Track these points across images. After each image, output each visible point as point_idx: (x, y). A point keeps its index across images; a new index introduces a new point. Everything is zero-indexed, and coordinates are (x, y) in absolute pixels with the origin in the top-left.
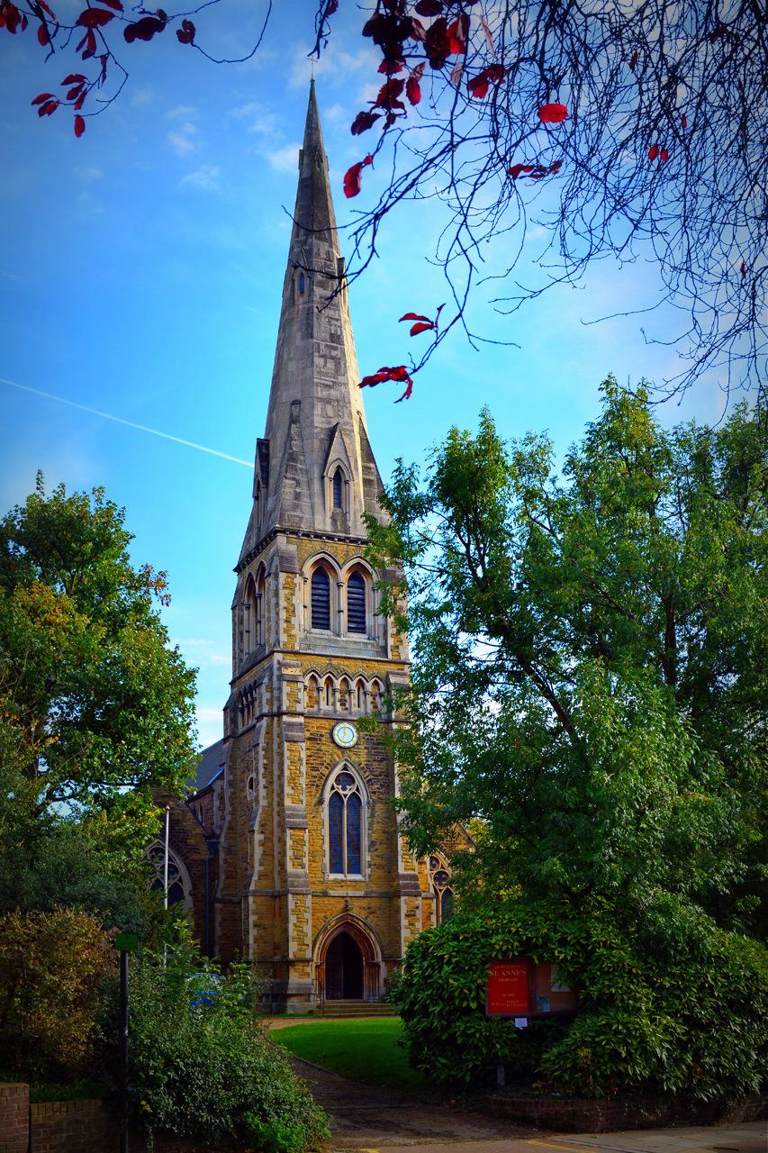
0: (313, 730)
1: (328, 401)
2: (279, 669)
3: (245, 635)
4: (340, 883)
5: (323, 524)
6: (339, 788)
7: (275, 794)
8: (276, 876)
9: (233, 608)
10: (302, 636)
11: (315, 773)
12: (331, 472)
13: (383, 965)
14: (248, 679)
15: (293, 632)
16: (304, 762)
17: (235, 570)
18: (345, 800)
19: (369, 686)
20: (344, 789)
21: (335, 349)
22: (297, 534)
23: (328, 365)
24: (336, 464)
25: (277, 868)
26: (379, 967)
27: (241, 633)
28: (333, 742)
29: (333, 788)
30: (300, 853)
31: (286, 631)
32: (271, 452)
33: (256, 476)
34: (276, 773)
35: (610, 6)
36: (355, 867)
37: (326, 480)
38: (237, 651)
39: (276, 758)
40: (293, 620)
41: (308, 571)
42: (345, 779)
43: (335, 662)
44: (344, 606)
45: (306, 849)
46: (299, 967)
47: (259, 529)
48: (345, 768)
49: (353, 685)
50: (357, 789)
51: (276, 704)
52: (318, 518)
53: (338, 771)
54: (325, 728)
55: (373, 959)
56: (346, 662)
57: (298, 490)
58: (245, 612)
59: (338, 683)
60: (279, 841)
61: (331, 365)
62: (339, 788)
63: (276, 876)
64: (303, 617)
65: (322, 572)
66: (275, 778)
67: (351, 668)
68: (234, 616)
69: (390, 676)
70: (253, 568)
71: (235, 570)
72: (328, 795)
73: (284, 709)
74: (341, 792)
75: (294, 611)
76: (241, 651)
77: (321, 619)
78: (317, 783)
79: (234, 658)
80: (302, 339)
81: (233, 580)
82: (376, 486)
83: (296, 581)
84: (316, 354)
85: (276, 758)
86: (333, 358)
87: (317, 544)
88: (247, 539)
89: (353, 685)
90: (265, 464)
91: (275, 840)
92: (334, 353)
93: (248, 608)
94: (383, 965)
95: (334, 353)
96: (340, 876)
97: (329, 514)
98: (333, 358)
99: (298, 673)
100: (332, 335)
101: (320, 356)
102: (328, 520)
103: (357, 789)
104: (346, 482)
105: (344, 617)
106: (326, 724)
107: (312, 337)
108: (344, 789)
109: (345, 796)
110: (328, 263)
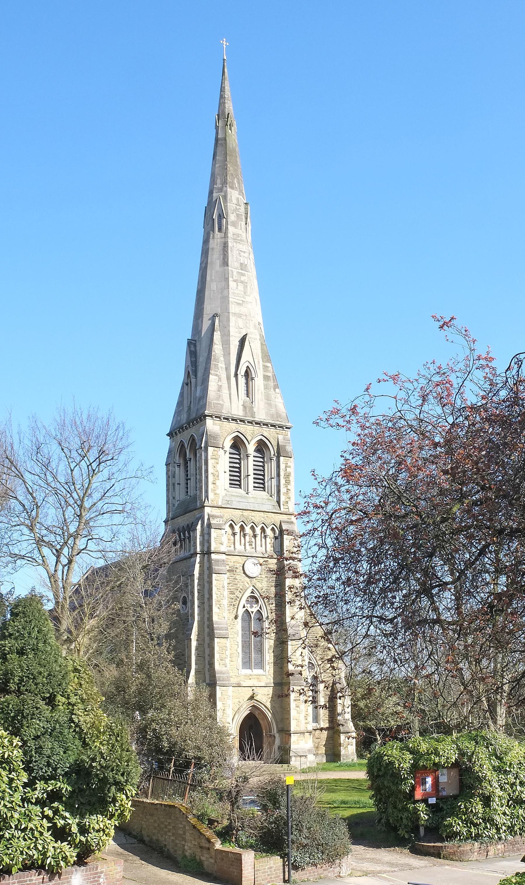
0: (231, 564)
1: (239, 315)
2: (209, 519)
3: (176, 485)
4: (250, 677)
5: (238, 411)
6: (248, 606)
7: (206, 612)
8: (207, 672)
9: (167, 465)
10: (224, 495)
11: (232, 596)
12: (242, 370)
13: (277, 735)
14: (182, 521)
15: (217, 492)
16: (226, 588)
17: (168, 435)
18: (252, 616)
19: (269, 532)
20: (252, 607)
21: (243, 275)
22: (219, 418)
23: (239, 288)
24: (247, 364)
25: (207, 666)
26: (275, 737)
27: (174, 484)
28: (244, 573)
29: (244, 607)
30: (224, 656)
31: (214, 490)
32: (198, 351)
33: (187, 367)
34: (206, 596)
35: (523, 584)
36: (260, 664)
37: (239, 376)
38: (171, 498)
39: (206, 585)
40: (217, 482)
41: (228, 443)
42: (254, 599)
43: (246, 513)
44: (251, 472)
45: (228, 653)
47: (189, 408)
49: (258, 531)
50: (260, 608)
51: (206, 545)
52: (234, 405)
53: (248, 593)
54: (239, 563)
55: (270, 732)
56: (253, 513)
57: (220, 384)
58: (177, 469)
59: (248, 530)
60: (209, 647)
61: (241, 287)
62: (248, 606)
63: (207, 672)
64: (224, 479)
65: (238, 445)
66: (206, 600)
67: (258, 518)
68: (168, 471)
69: (283, 524)
70: (185, 437)
71: (168, 435)
72: (241, 611)
73: (213, 549)
74: (250, 610)
75: (218, 476)
76: (174, 498)
77: (236, 480)
78: (234, 603)
79: (168, 502)
80: (220, 266)
81: (166, 443)
82: (272, 381)
83: (219, 453)
84: (230, 279)
85: (206, 585)
86: (242, 282)
87: (233, 426)
88: (178, 413)
89: (258, 531)
90: (193, 359)
91: (206, 645)
92: (243, 278)
93: (179, 466)
94: (277, 735)
95: (243, 278)
96: (248, 671)
97: (241, 403)
98: (242, 282)
99: (221, 522)
100: (241, 264)
101: (235, 281)
102: (241, 408)
103: (260, 608)
104: (252, 379)
105: (251, 479)
106: (241, 560)
107: (228, 265)
108: (252, 607)
109: (252, 612)
110: (238, 207)
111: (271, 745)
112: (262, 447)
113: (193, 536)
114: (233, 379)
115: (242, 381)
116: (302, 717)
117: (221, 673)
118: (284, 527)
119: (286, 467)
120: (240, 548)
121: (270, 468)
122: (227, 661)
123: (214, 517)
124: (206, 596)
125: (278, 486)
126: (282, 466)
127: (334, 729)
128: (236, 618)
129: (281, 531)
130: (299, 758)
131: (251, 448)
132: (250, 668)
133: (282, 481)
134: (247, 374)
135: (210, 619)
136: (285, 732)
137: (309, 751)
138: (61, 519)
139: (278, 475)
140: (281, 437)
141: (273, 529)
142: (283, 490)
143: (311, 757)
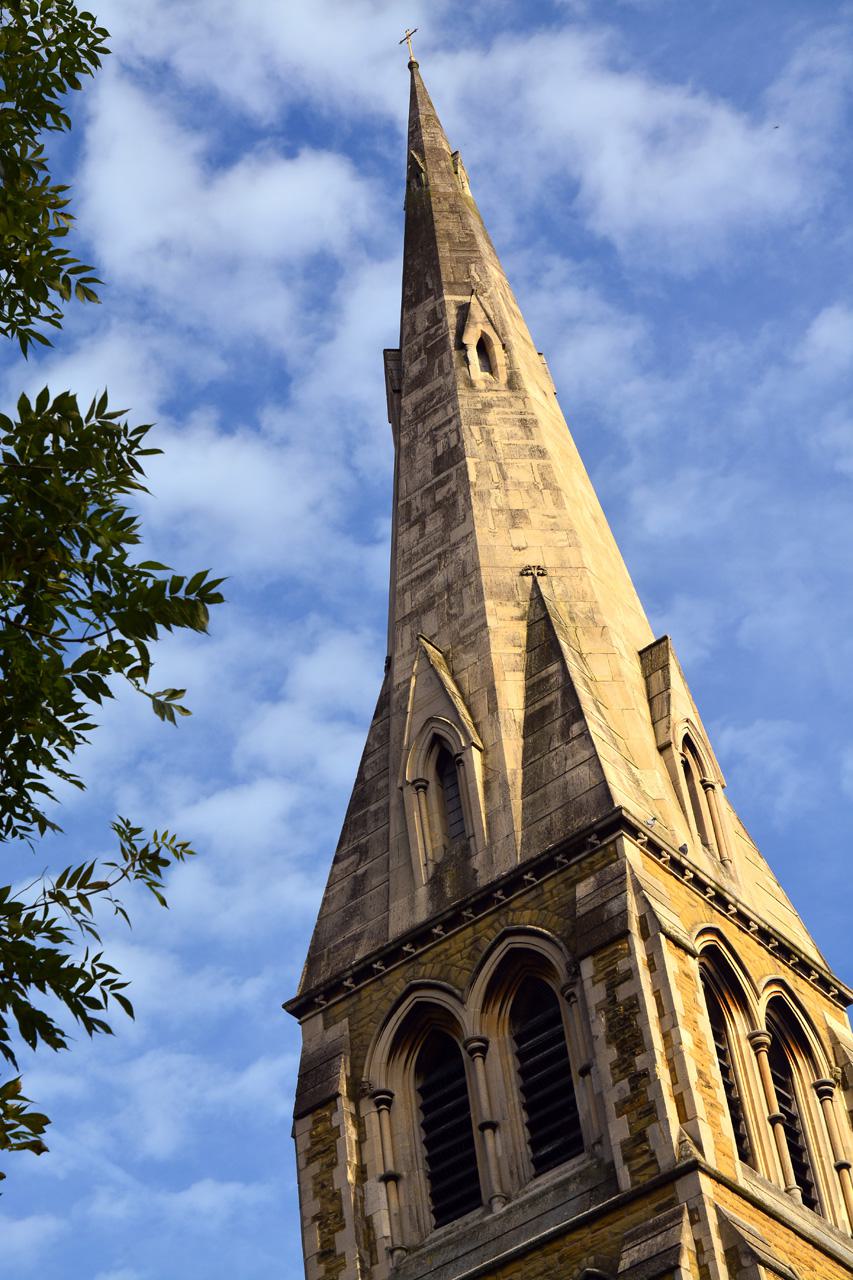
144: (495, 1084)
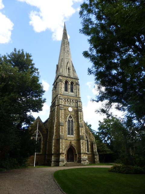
6: (69, 119)
19: (74, 101)
36: (72, 134)
42: (70, 117)
43: (68, 97)
45: (63, 130)
46: (62, 155)
48: (70, 115)
49: (71, 101)
53: (69, 116)
56: (70, 97)
59: (69, 100)
61: (67, 54)
62: (69, 119)
64: (63, 89)
65: (66, 82)
67: (71, 98)
73: (60, 104)
77: (66, 90)
78: (65, 118)
87: (66, 78)
89: (71, 101)
91: (58, 129)
96: (69, 136)
97: (67, 74)
105: (70, 90)
111: (76, 157)
112: (72, 83)
113: (80, 115)
114: (65, 70)
115: (67, 70)
116: (84, 149)
117: (62, 135)
118: (78, 100)
119: (78, 87)
120: (67, 104)
121: (74, 87)
122: (63, 132)
123: (60, 97)
124: (58, 116)
125: (76, 92)
126: (77, 87)
127: (93, 154)
128: (66, 121)
129: (77, 101)
130: (83, 161)
131: (70, 83)
132: (70, 135)
133: (77, 90)
134: (69, 69)
135: (59, 121)
136: (80, 153)
137: (87, 159)
138: (76, 105)
139: (76, 89)
140: (76, 81)
141: (75, 101)
142: (77, 92)
143: (87, 161)
144: (69, 87)
